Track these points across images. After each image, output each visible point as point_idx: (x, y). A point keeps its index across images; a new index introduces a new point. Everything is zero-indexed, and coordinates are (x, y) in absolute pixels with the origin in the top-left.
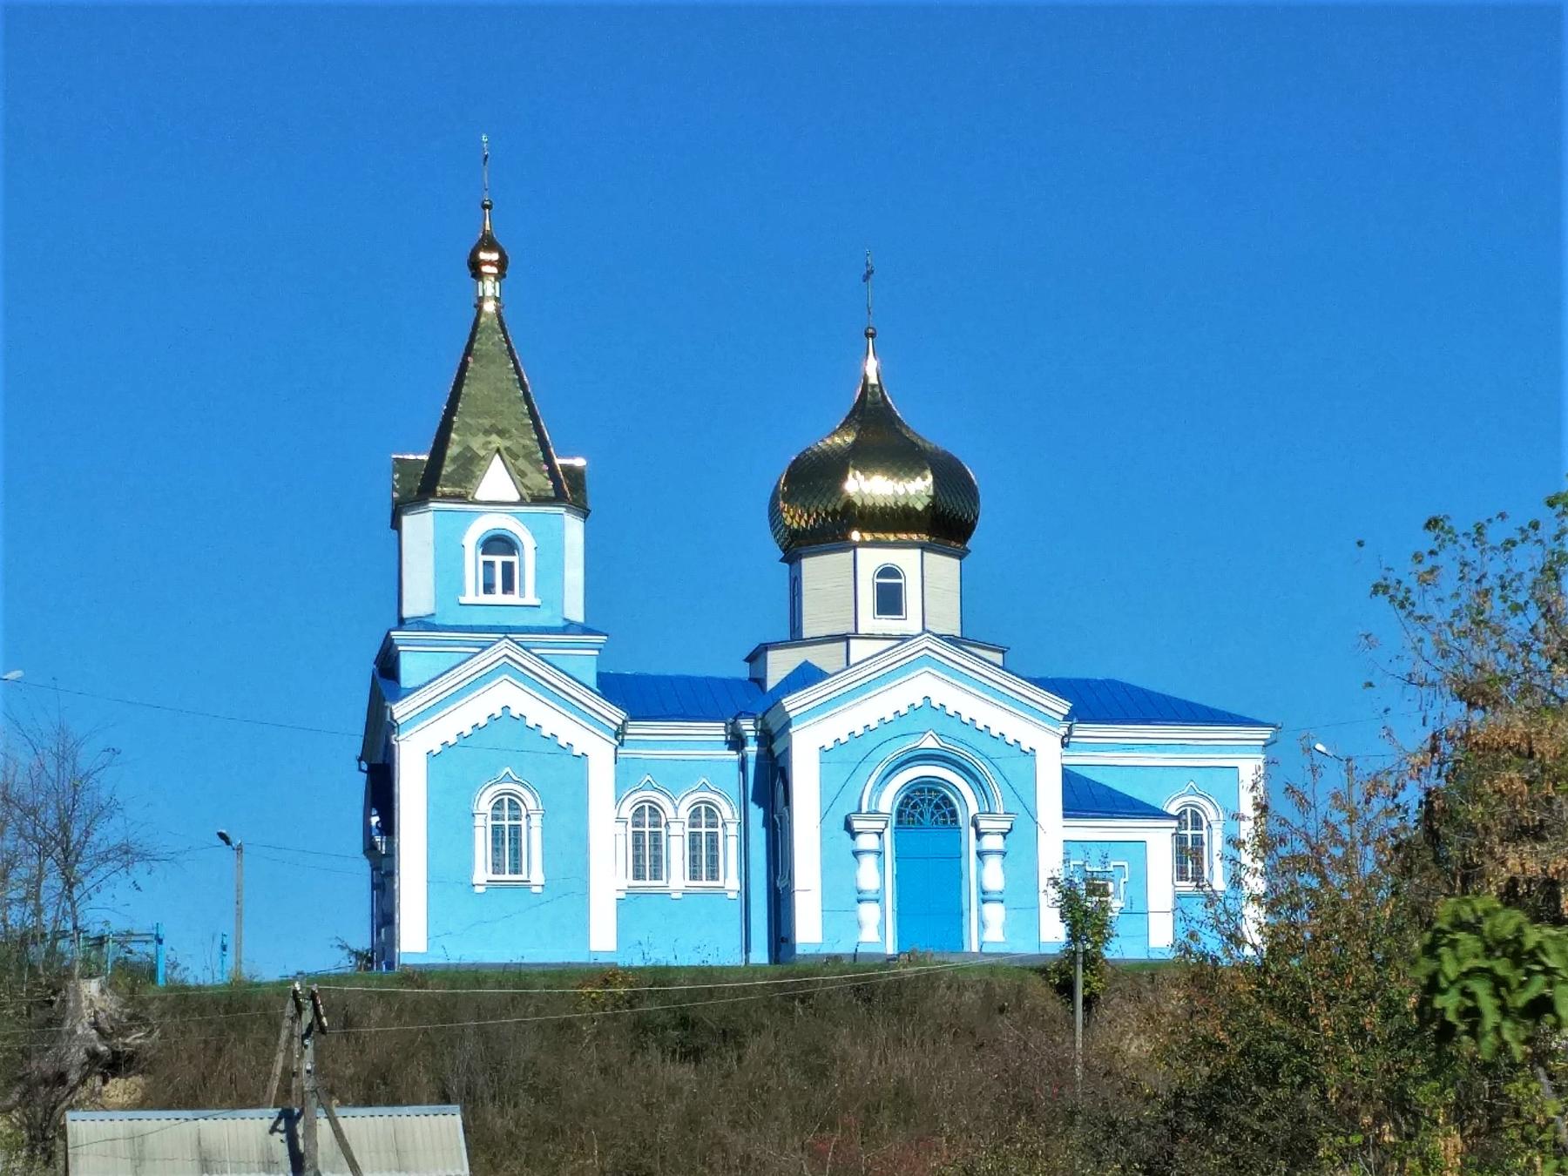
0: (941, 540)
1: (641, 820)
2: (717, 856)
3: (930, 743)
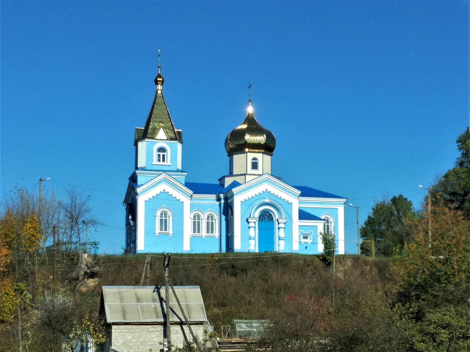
0: (267, 151)
3: (267, 201)
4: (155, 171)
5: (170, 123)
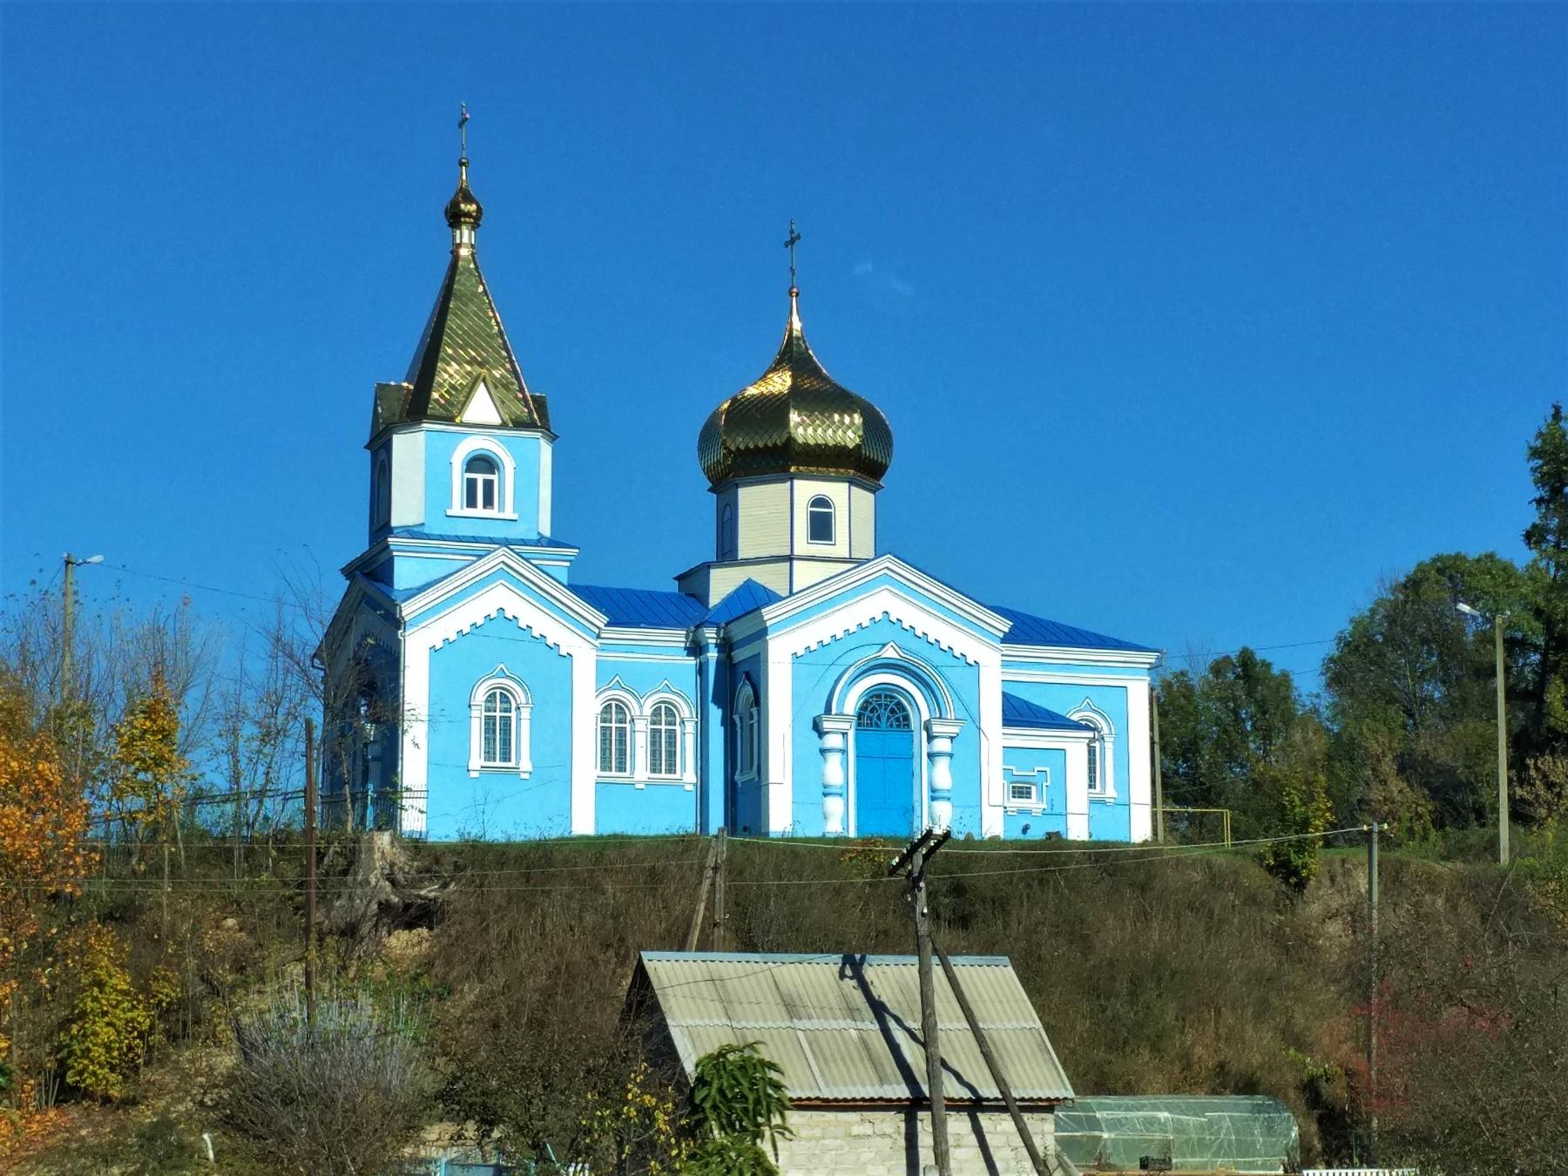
1: (609, 717)
2: (675, 752)
3: (890, 653)
4: (458, 539)
5: (508, 366)
